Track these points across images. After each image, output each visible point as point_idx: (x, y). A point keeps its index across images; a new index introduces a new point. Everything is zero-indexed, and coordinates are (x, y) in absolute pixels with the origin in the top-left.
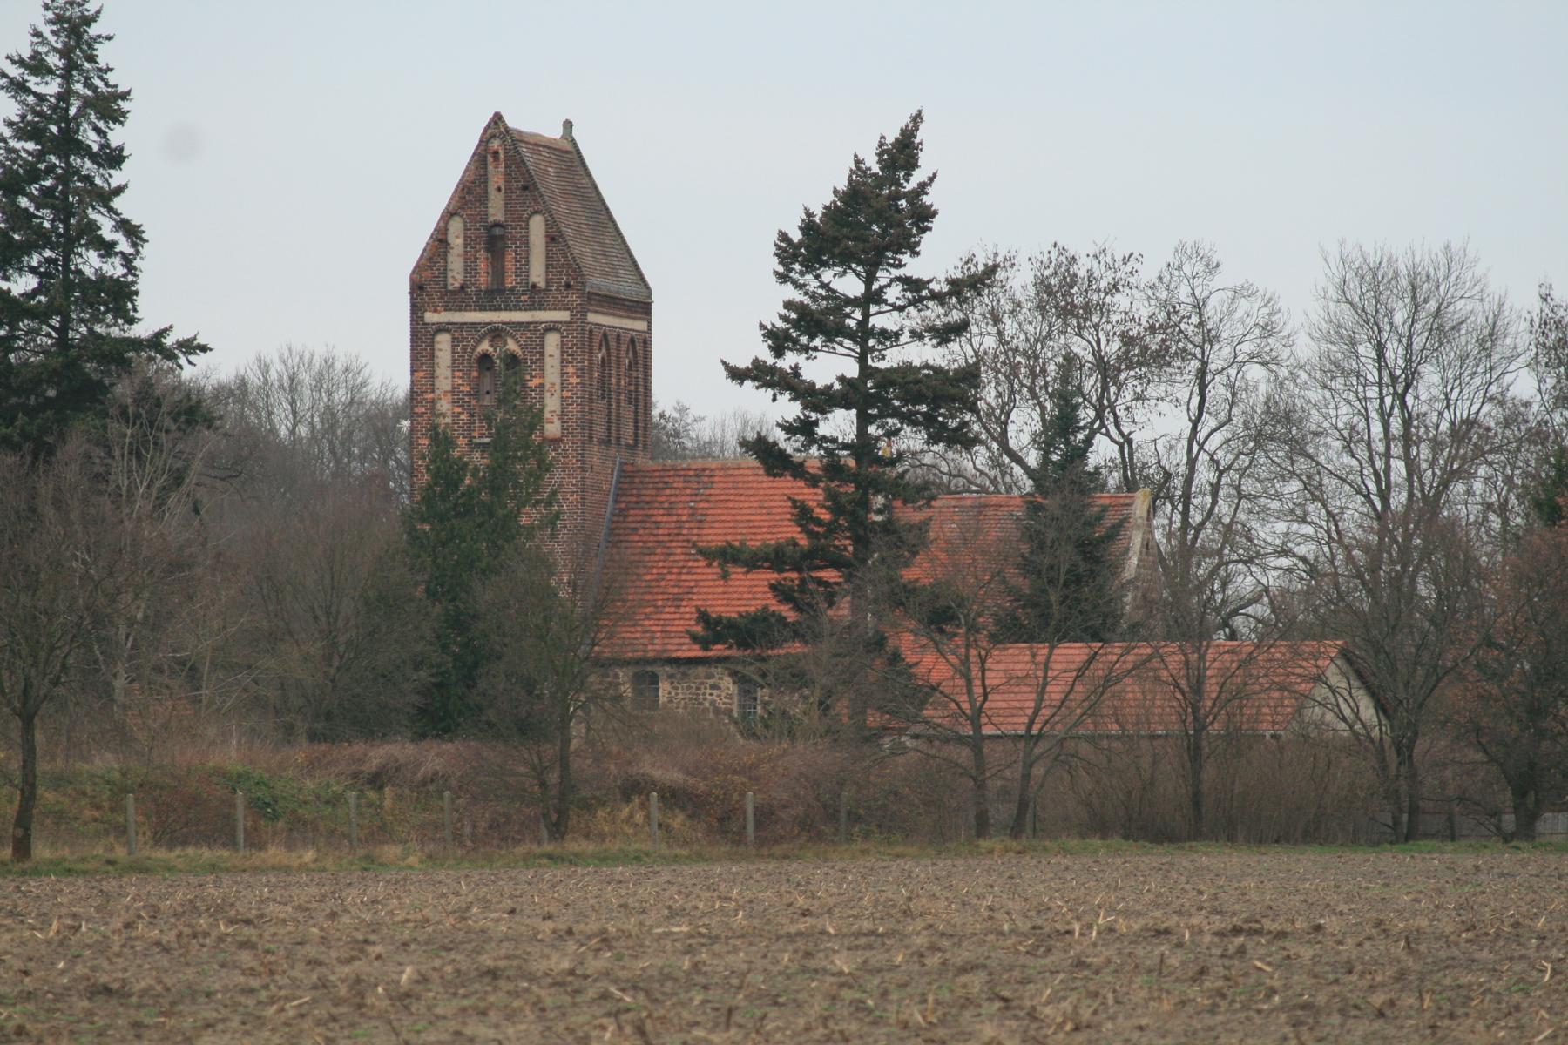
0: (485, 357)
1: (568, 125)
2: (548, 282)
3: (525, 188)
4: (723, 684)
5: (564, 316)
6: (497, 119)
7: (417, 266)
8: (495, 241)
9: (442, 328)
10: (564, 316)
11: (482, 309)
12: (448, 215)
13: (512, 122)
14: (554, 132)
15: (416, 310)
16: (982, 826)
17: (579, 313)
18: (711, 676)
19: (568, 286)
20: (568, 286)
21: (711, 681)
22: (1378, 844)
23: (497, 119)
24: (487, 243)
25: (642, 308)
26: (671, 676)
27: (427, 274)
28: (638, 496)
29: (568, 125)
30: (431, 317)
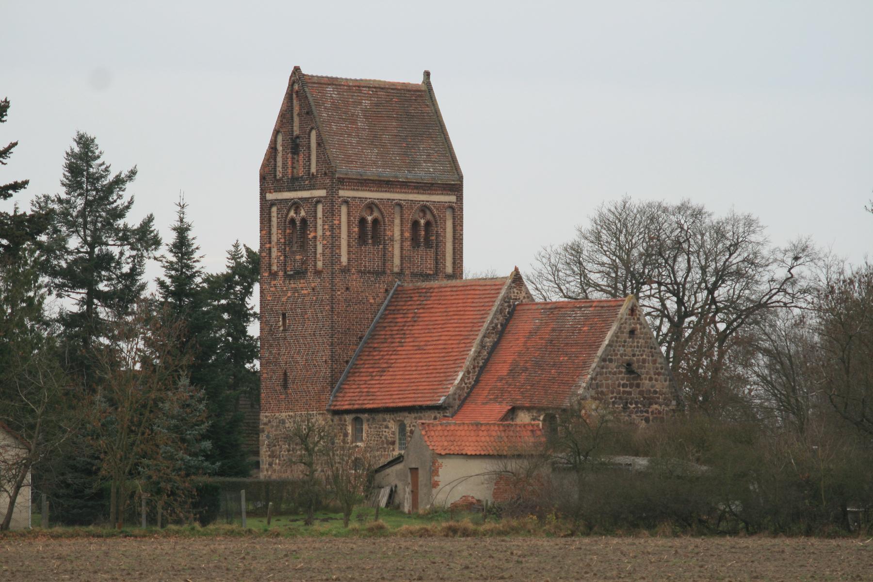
0: (293, 221)
1: (427, 74)
2: (317, 171)
3: (308, 113)
4: (390, 425)
5: (322, 193)
6: (297, 69)
7: (263, 165)
8: (295, 146)
9: (273, 203)
10: (322, 193)
11: (289, 190)
12: (276, 132)
13: (304, 71)
14: (417, 80)
15: (263, 192)
16: (133, 518)
17: (332, 191)
18: (384, 420)
19: (325, 174)
20: (325, 174)
21: (385, 423)
22: (636, 526)
23: (297, 69)
24: (292, 148)
25: (456, 188)
26: (368, 420)
27: (266, 170)
28: (396, 306)
29: (427, 74)
30: (270, 196)
